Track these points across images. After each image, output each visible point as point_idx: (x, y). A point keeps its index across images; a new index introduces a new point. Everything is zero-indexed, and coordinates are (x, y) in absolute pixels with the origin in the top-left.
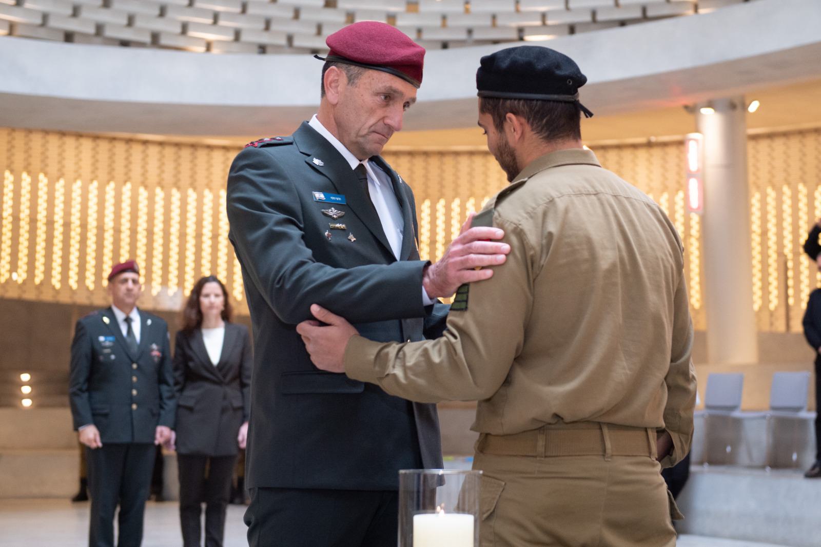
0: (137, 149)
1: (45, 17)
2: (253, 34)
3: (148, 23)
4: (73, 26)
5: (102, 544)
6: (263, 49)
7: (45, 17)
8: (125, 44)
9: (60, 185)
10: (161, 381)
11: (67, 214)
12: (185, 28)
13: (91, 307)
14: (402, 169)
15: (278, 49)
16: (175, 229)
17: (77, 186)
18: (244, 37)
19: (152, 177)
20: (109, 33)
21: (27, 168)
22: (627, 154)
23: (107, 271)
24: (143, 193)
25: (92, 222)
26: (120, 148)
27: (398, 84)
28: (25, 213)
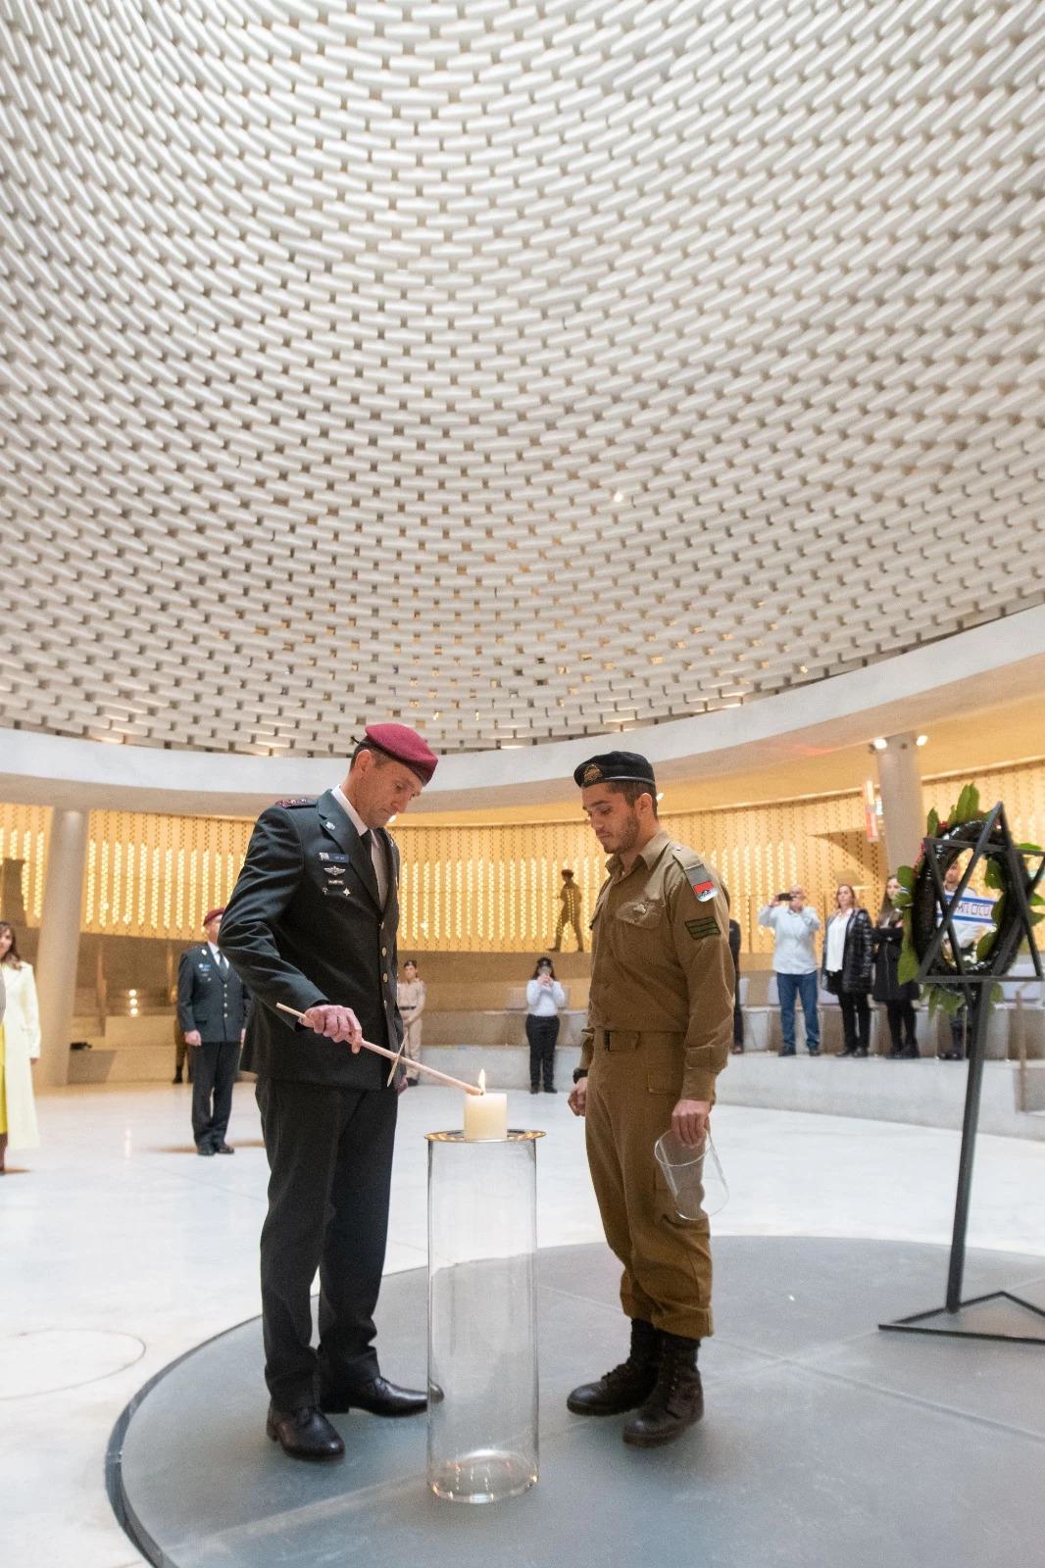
0: (214, 826)
1: (150, 731)
2: (304, 742)
3: (226, 735)
4: (171, 737)
5: (202, 1115)
6: (311, 754)
7: (150, 731)
8: (209, 750)
9: (156, 852)
10: (245, 996)
11: (162, 873)
12: (253, 739)
13: (191, 944)
14: (398, 840)
15: (322, 754)
16: (512, 908)
17: (169, 853)
18: (297, 746)
19: (225, 847)
20: (197, 742)
21: (132, 840)
22: (571, 829)
23: (204, 913)
24: (219, 858)
25: (130, 874)
26: (201, 825)
27: (413, 778)
28: (130, 874)
